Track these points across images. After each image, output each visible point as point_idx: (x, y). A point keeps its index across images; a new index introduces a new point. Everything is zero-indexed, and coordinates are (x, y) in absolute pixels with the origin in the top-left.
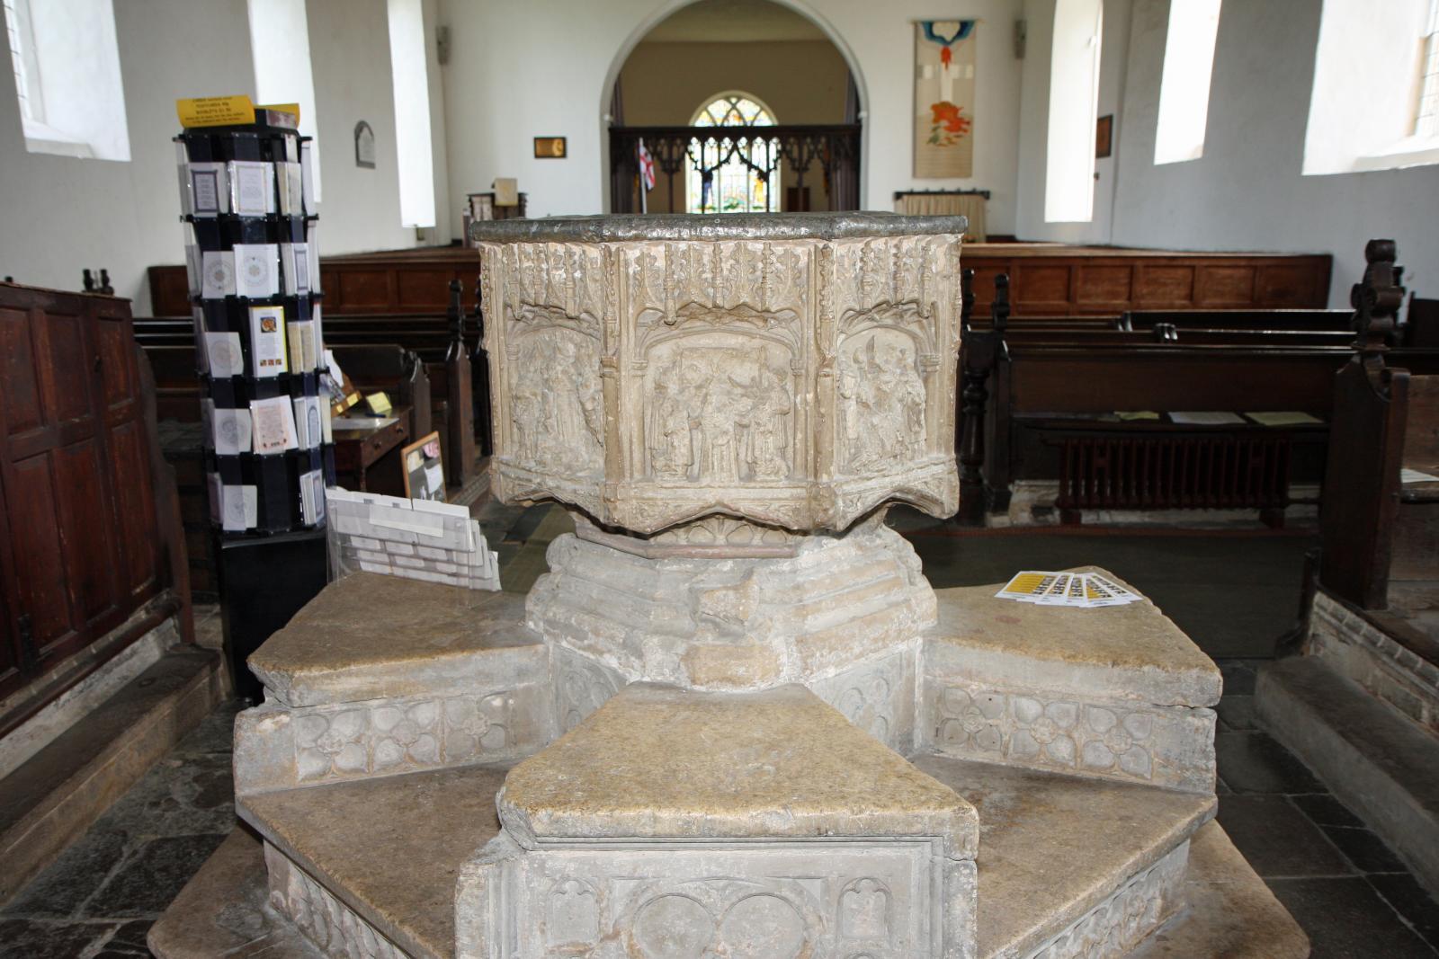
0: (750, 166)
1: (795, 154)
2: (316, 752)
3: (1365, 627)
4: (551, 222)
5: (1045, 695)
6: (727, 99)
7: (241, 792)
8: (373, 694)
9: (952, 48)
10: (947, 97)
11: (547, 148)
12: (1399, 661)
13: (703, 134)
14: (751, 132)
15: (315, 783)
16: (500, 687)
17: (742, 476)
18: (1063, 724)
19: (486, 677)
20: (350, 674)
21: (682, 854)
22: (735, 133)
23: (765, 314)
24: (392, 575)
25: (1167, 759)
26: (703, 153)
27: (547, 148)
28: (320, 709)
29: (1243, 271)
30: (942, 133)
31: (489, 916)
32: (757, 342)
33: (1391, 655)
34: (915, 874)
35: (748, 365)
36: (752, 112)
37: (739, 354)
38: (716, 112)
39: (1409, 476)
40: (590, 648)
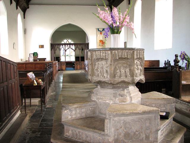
0: (72, 49)
1: (79, 47)
2: (70, 115)
3: (180, 101)
4: (125, 45)
5: (155, 103)
6: (66, 39)
7: (63, 120)
8: (78, 107)
9: (102, 32)
10: (101, 39)
11: (42, 47)
12: (184, 104)
13: (63, 44)
14: (70, 44)
15: (71, 119)
16: (91, 107)
17: (96, 87)
18: (158, 107)
19: (90, 105)
20: (75, 105)
21: (129, 117)
22: (67, 44)
23: (128, 59)
24: (8, 118)
25: (170, 109)
26: (62, 48)
27: (42, 47)
28: (72, 109)
29: (148, 63)
30: (101, 44)
31: (108, 125)
32: (126, 62)
33: (183, 103)
34: (153, 118)
35: (125, 65)
36: (70, 41)
37: (124, 63)
38: (65, 41)
39: (184, 82)
40: (104, 100)
